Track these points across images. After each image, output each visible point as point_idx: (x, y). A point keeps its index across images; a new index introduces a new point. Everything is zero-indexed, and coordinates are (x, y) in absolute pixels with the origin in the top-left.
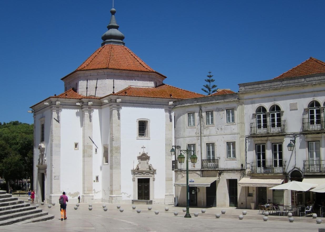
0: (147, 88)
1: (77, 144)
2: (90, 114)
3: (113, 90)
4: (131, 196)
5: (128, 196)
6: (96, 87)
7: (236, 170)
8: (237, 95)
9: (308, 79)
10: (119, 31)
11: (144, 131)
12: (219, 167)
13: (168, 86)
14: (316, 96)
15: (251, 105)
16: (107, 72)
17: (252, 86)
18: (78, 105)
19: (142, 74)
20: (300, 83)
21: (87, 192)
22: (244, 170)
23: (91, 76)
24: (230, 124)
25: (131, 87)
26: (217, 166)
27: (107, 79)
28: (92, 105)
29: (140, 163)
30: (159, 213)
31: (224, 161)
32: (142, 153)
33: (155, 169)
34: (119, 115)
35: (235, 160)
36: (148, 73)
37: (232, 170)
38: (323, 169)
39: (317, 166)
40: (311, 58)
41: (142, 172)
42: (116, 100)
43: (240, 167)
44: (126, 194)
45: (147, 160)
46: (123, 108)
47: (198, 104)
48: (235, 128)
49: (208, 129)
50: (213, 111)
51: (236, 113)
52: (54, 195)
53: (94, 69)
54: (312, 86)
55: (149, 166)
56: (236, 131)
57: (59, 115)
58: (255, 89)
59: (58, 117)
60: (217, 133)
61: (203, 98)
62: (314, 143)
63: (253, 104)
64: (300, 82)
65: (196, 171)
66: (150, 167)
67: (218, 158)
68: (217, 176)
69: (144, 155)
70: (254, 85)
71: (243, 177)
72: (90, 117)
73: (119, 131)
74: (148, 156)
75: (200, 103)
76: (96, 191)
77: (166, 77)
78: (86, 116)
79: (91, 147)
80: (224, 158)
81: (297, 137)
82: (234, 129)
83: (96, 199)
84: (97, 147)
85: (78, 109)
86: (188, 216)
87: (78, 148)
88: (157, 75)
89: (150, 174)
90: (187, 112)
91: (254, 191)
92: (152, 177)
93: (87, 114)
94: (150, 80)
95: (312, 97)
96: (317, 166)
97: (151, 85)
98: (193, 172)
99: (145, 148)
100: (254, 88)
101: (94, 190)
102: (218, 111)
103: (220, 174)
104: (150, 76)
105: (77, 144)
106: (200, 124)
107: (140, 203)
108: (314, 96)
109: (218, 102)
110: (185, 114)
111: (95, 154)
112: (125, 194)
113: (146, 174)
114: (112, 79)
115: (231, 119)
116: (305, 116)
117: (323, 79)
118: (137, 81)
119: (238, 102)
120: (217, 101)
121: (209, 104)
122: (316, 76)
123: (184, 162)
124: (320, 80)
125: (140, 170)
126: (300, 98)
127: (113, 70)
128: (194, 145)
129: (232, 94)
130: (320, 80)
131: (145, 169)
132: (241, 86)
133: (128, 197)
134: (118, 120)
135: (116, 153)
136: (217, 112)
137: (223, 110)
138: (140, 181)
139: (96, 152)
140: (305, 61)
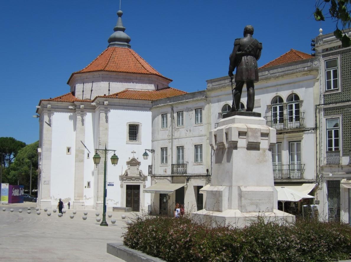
0: (146, 91)
1: (70, 148)
2: (82, 117)
3: (108, 93)
4: (119, 203)
5: (115, 203)
6: (92, 90)
7: (203, 176)
8: (205, 93)
9: (271, 72)
10: (126, 33)
11: (135, 135)
12: (187, 173)
13: (174, 89)
14: (279, 91)
15: (217, 104)
16: (102, 74)
17: (219, 82)
18: (71, 108)
19: (140, 76)
20: (263, 77)
21: (78, 198)
22: (210, 176)
23: (87, 78)
24: (198, 125)
25: (129, 90)
26: (186, 173)
27: (102, 81)
28: (84, 109)
29: (129, 168)
30: (116, 221)
31: (192, 166)
32: (131, 158)
33: (146, 176)
34: (107, 118)
35: (201, 165)
37: (198, 176)
38: (285, 175)
39: (279, 172)
40: (292, 51)
41: (131, 178)
42: (104, 103)
43: (205, 172)
44: (112, 201)
45: (138, 166)
46: (112, 111)
47: (170, 103)
48: (202, 129)
49: (178, 131)
50: (183, 111)
51: (203, 112)
52: (43, 201)
53: (89, 72)
54: (275, 79)
55: (139, 172)
56: (203, 133)
57: (51, 118)
58: (221, 85)
59: (50, 121)
60: (186, 135)
61: (175, 98)
63: (219, 103)
64: (264, 75)
65: (167, 176)
66: (140, 173)
67: (187, 162)
68: (186, 182)
69: (134, 160)
70: (220, 80)
71: (208, 184)
72: (83, 121)
73: (107, 134)
74: (139, 161)
75: (172, 103)
76: (88, 198)
77: (172, 81)
78: (78, 120)
79: (83, 152)
80: (192, 162)
82: (201, 131)
83: (87, 206)
84: (89, 151)
85: (71, 112)
87: (71, 153)
88: (158, 78)
89: (140, 181)
90: (161, 113)
92: (143, 184)
93: (79, 117)
94: (150, 82)
95: (275, 92)
96: (279, 172)
97: (151, 87)
98: (164, 178)
99: (135, 152)
100: (221, 84)
101: (85, 196)
102: (188, 111)
103: (188, 180)
104: (150, 78)
105: (70, 148)
106: (171, 127)
107: (119, 210)
108: (278, 91)
109: (187, 101)
110: (159, 116)
111: (88, 158)
112: (111, 201)
113: (136, 180)
114: (107, 82)
115: (199, 120)
116: (267, 114)
117: (286, 71)
118: (135, 84)
119: (205, 101)
120: (187, 100)
121: (179, 103)
122: (280, 68)
123: (117, 164)
124: (283, 72)
125: (129, 175)
126: (264, 93)
127: (108, 72)
128: (166, 148)
129: (201, 93)
130: (283, 72)
131: (135, 175)
132: (209, 83)
133: (115, 204)
134: (106, 124)
136: (187, 112)
137: (192, 110)
138: (129, 187)
139: (88, 157)
140: (285, 54)
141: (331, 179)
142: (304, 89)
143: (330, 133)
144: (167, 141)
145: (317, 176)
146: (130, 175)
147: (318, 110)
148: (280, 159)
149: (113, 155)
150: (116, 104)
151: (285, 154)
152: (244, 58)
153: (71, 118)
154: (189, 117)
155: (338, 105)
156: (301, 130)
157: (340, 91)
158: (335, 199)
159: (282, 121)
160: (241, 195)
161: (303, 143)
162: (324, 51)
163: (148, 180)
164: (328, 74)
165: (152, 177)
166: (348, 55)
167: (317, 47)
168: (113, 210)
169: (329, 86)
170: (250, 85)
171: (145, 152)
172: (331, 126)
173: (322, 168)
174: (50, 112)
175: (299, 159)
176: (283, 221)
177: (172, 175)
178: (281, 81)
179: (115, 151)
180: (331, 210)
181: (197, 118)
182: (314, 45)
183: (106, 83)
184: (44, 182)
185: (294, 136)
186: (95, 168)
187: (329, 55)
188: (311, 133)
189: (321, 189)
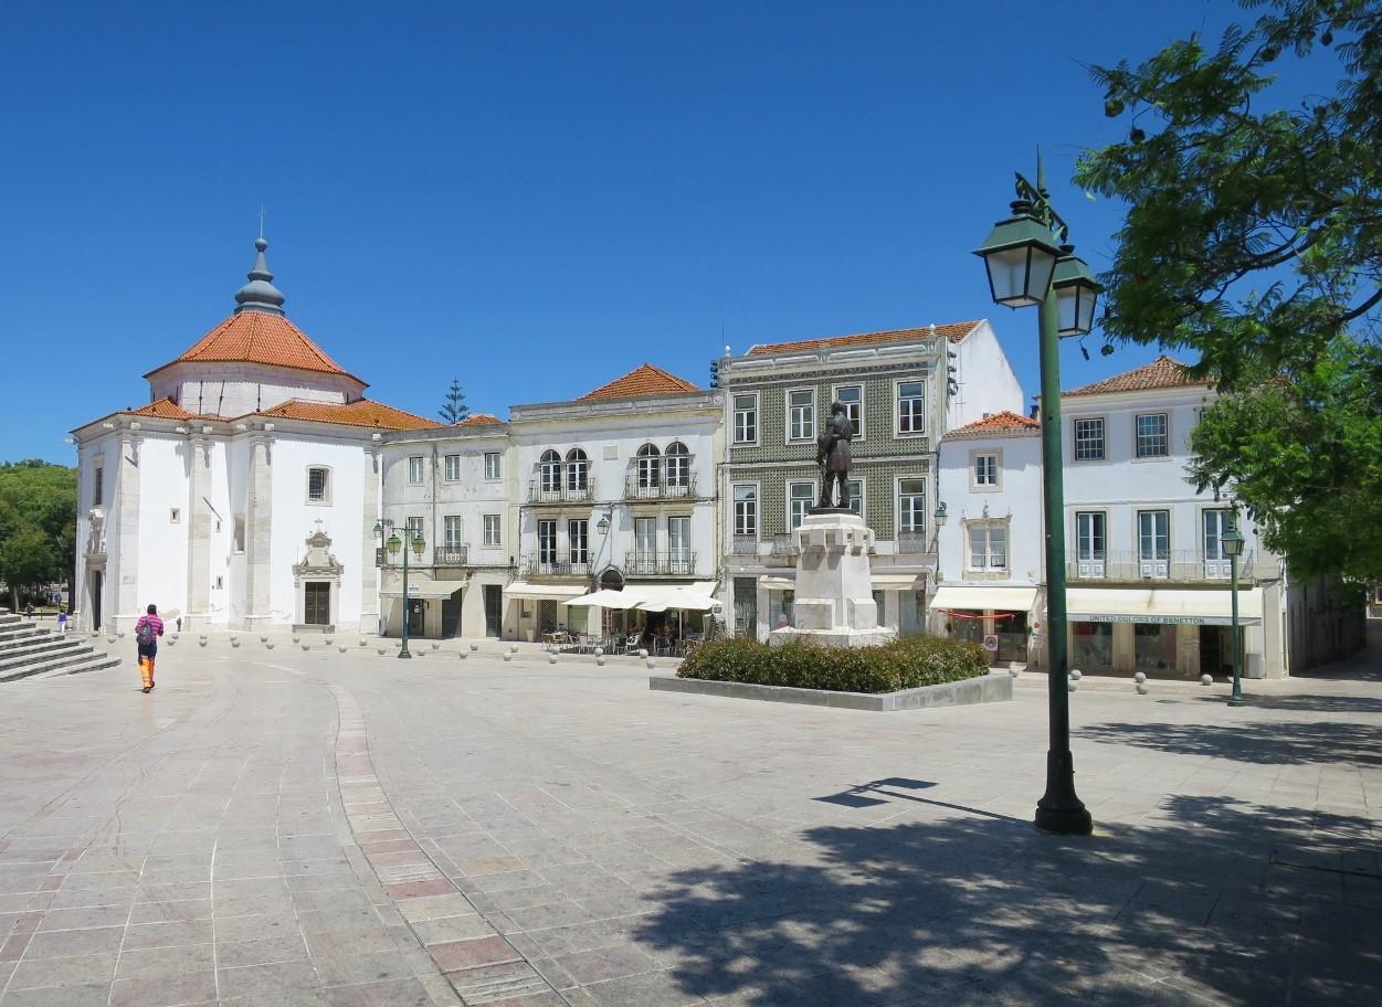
6: (221, 398)
9: (638, 404)
15: (531, 447)
24: (491, 481)
32: (314, 532)
34: (269, 455)
37: (492, 568)
41: (315, 570)
42: (263, 426)
43: (507, 563)
48: (499, 489)
56: (501, 495)
59: (135, 455)
66: (331, 560)
70: (538, 408)
73: (269, 487)
77: (368, 386)
79: (208, 519)
86: (405, 654)
93: (199, 450)
94: (335, 388)
97: (337, 398)
101: (213, 605)
103: (469, 575)
108: (649, 435)
115: (493, 473)
129: (497, 425)
137: (478, 454)
138: (310, 587)
141: (741, 576)
142: (697, 436)
143: (740, 508)
144: (425, 506)
145: (718, 571)
146: (312, 563)
147: (720, 472)
148: (653, 543)
150: (286, 430)
151: (662, 536)
152: (839, 442)
153: (178, 450)
154: (472, 467)
155: (755, 465)
156: (691, 499)
157: (758, 445)
158: (747, 605)
159: (655, 483)
160: (852, 610)
161: (693, 519)
162: (732, 381)
163: (499, 583)
164: (739, 417)
165: (382, 569)
167: (722, 374)
168: (294, 631)
169: (740, 435)
170: (842, 479)
172: (742, 495)
173: (726, 559)
174: (136, 438)
175: (687, 543)
178: (656, 420)
180: (739, 621)
181: (490, 469)
182: (716, 371)
183: (254, 386)
185: (680, 508)
186: (233, 549)
187: (741, 389)
188: (709, 505)
189: (724, 590)
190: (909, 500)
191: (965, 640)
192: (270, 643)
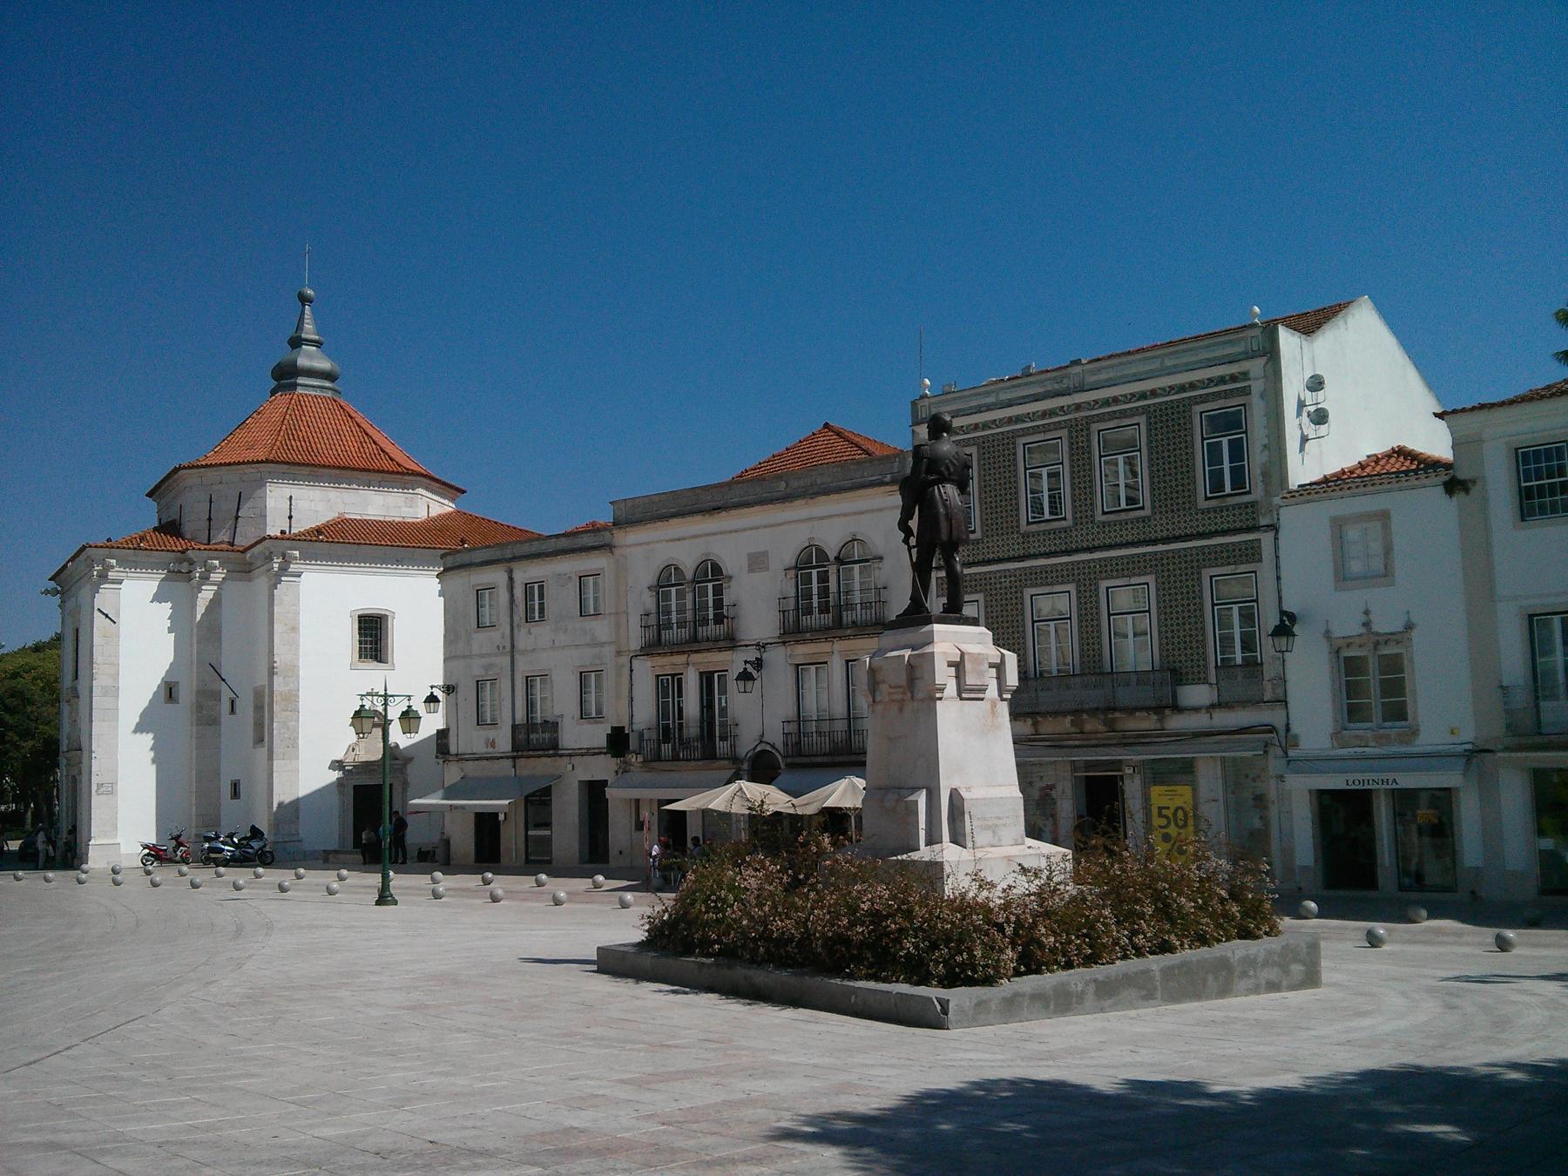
12: (560, 747)
19: (380, 479)
36: (401, 477)
48: (601, 629)
52: (99, 843)
62: (813, 668)
73: (294, 645)
77: (464, 492)
79: (216, 696)
81: (1141, 677)
86: (384, 898)
91: (653, 814)
123: (417, 733)
135: (283, 710)
149: (405, 709)
166: (1165, 485)
171: (429, 694)
176: (265, 846)
177: (515, 754)
179: (409, 696)
184: (98, 789)
190: (1051, 513)
191: (959, 916)
192: (119, 877)
